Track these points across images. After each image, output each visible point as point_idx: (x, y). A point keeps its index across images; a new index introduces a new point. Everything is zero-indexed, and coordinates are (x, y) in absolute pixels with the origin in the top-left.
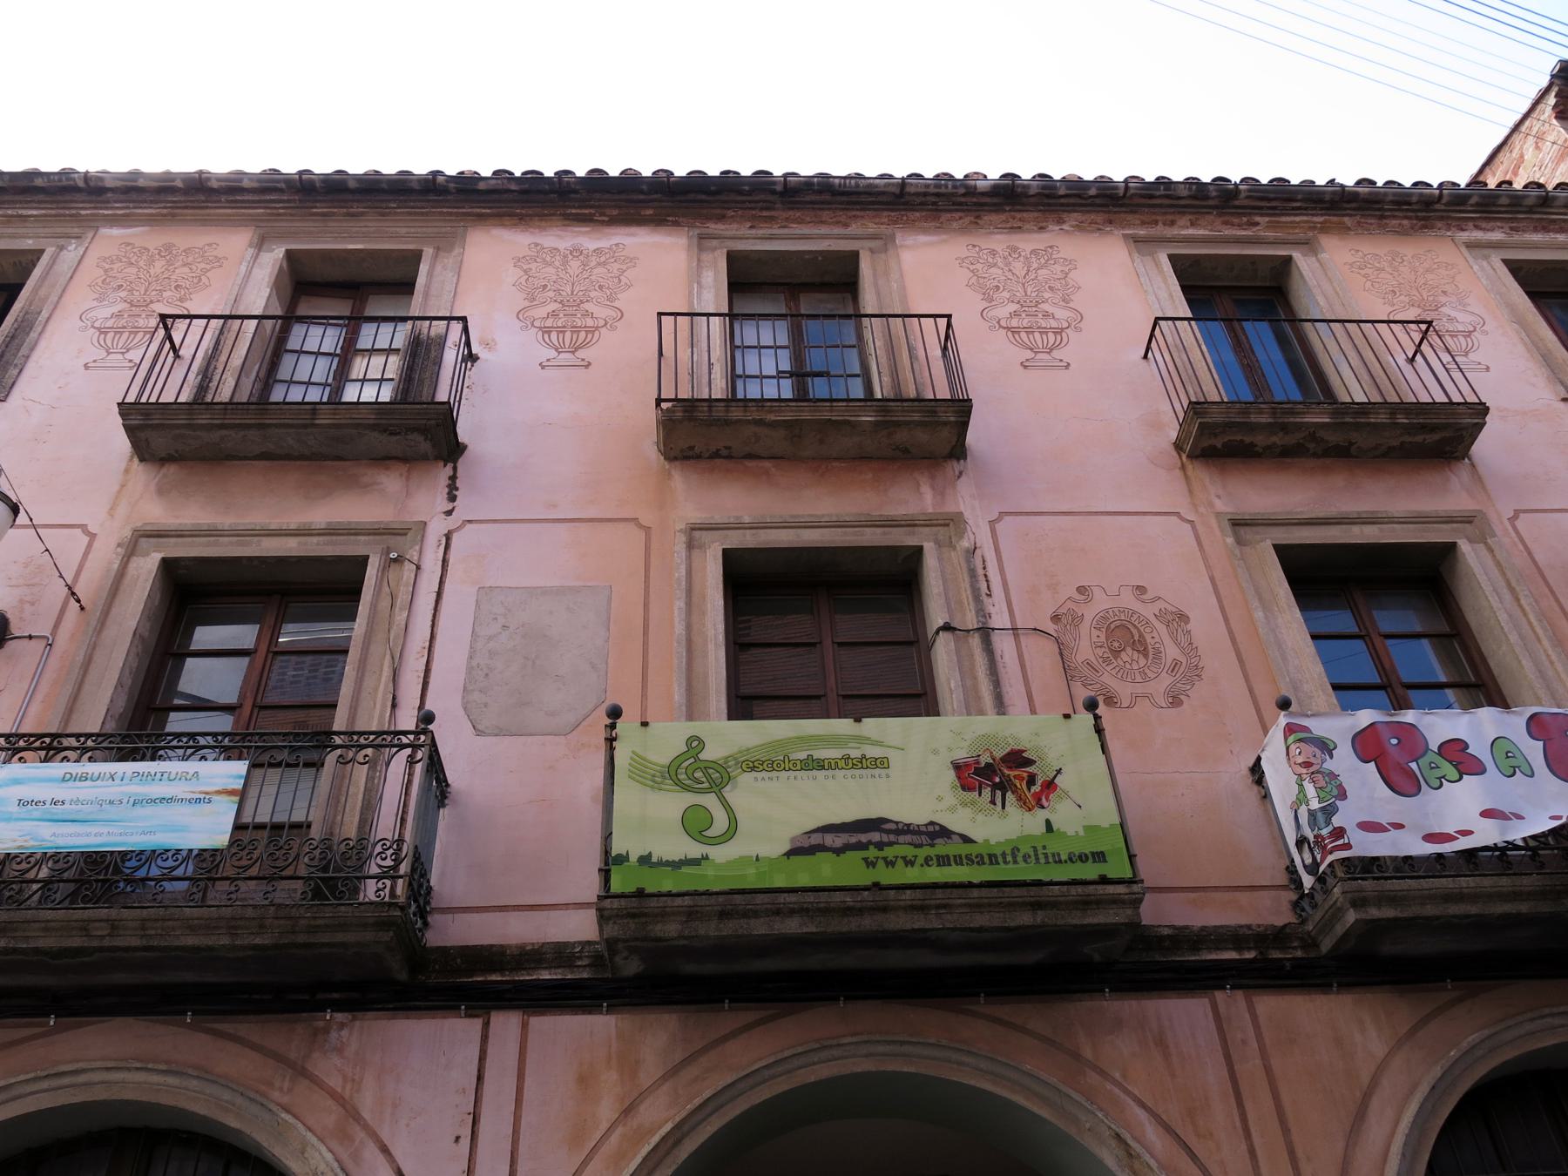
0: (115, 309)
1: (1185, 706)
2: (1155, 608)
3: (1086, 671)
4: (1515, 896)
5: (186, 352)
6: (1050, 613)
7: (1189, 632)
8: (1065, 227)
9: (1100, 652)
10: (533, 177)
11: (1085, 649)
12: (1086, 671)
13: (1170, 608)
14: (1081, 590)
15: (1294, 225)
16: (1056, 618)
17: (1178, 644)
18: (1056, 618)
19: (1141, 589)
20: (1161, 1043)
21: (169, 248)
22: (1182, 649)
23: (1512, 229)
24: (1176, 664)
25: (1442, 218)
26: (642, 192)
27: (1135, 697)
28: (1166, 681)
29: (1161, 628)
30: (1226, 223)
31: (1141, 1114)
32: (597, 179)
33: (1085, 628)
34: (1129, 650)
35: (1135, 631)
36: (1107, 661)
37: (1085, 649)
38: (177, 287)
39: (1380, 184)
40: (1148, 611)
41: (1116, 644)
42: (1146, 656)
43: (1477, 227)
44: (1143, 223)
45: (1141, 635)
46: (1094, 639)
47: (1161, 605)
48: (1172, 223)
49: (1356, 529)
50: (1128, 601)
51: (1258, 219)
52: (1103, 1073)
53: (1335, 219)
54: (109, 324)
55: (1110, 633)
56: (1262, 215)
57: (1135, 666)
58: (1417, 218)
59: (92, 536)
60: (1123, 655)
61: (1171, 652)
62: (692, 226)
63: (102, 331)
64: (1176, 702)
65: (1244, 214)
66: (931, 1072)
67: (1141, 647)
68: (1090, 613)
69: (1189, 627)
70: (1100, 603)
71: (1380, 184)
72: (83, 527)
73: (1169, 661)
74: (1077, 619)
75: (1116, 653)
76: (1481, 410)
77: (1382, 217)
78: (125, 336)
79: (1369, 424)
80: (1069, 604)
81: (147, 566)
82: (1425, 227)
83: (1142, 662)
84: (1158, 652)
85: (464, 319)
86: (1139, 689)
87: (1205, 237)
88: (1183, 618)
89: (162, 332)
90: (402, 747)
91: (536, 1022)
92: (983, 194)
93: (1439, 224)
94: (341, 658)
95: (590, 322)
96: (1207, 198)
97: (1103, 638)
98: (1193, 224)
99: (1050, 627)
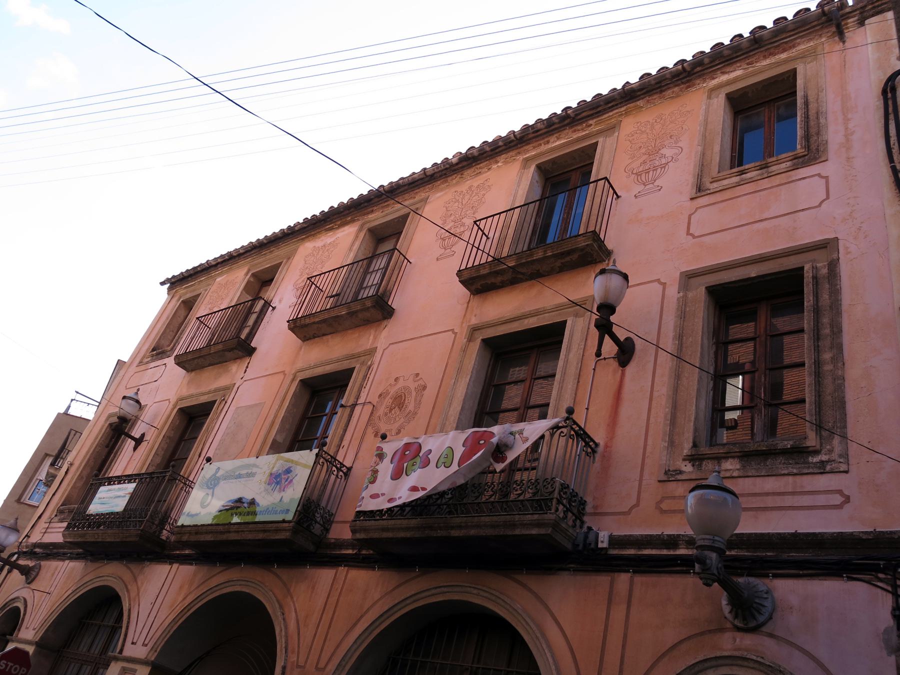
0: (641, 160)
4: (408, 529)
5: (491, 236)
8: (499, 164)
10: (342, 205)
15: (610, 118)
20: (313, 588)
21: (470, 187)
23: (748, 64)
25: (700, 77)
26: (500, 147)
30: (575, 131)
31: (294, 614)
32: (700, 58)
38: (671, 137)
39: (790, 17)
43: (723, 73)
44: (534, 147)
48: (548, 142)
49: (526, 321)
51: (591, 122)
52: (292, 598)
53: (632, 105)
54: (641, 169)
56: (593, 119)
58: (683, 83)
59: (664, 284)
62: (353, 221)
63: (638, 174)
65: (584, 122)
66: (461, 598)
71: (790, 17)
72: (658, 281)
77: (661, 92)
78: (651, 173)
79: (537, 260)
81: (699, 293)
82: (689, 87)
85: (606, 178)
87: (737, 76)
89: (476, 228)
91: (181, 567)
92: (457, 164)
93: (698, 81)
95: (664, 161)
96: (554, 124)
98: (558, 139)
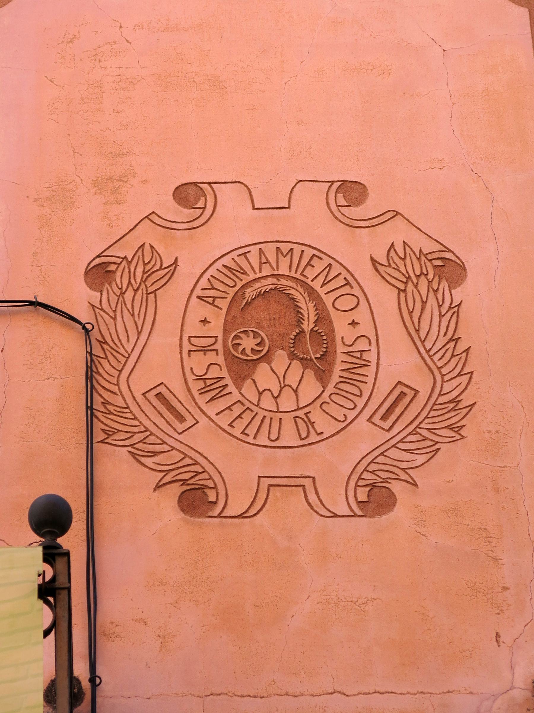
1: (399, 511)
2: (376, 243)
3: (152, 418)
6: (87, 256)
7: (456, 309)
9: (198, 363)
11: (160, 358)
12: (152, 418)
13: (419, 243)
14: (187, 194)
16: (99, 273)
17: (415, 335)
18: (99, 273)
19: (352, 191)
22: (425, 355)
24: (402, 394)
27: (272, 486)
28: (365, 438)
29: (383, 297)
33: (172, 299)
34: (281, 359)
35: (308, 310)
36: (213, 389)
37: (160, 358)
40: (354, 251)
41: (248, 343)
42: (323, 376)
45: (323, 317)
46: (193, 328)
47: (396, 233)
50: (312, 224)
55: (240, 309)
57: (287, 402)
60: (264, 376)
61: (397, 362)
64: (376, 499)
67: (315, 350)
68: (196, 256)
69: (458, 294)
70: (233, 228)
73: (384, 386)
74: (157, 273)
75: (242, 368)
76: (69, 551)
80: (148, 235)
83: (310, 388)
84: (359, 363)
86: (283, 465)
88: (449, 269)
90: (92, 375)
94: (302, 334)
97: (216, 327)
99: (79, 299)
